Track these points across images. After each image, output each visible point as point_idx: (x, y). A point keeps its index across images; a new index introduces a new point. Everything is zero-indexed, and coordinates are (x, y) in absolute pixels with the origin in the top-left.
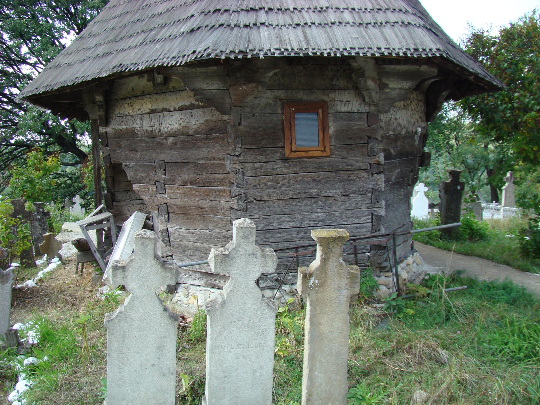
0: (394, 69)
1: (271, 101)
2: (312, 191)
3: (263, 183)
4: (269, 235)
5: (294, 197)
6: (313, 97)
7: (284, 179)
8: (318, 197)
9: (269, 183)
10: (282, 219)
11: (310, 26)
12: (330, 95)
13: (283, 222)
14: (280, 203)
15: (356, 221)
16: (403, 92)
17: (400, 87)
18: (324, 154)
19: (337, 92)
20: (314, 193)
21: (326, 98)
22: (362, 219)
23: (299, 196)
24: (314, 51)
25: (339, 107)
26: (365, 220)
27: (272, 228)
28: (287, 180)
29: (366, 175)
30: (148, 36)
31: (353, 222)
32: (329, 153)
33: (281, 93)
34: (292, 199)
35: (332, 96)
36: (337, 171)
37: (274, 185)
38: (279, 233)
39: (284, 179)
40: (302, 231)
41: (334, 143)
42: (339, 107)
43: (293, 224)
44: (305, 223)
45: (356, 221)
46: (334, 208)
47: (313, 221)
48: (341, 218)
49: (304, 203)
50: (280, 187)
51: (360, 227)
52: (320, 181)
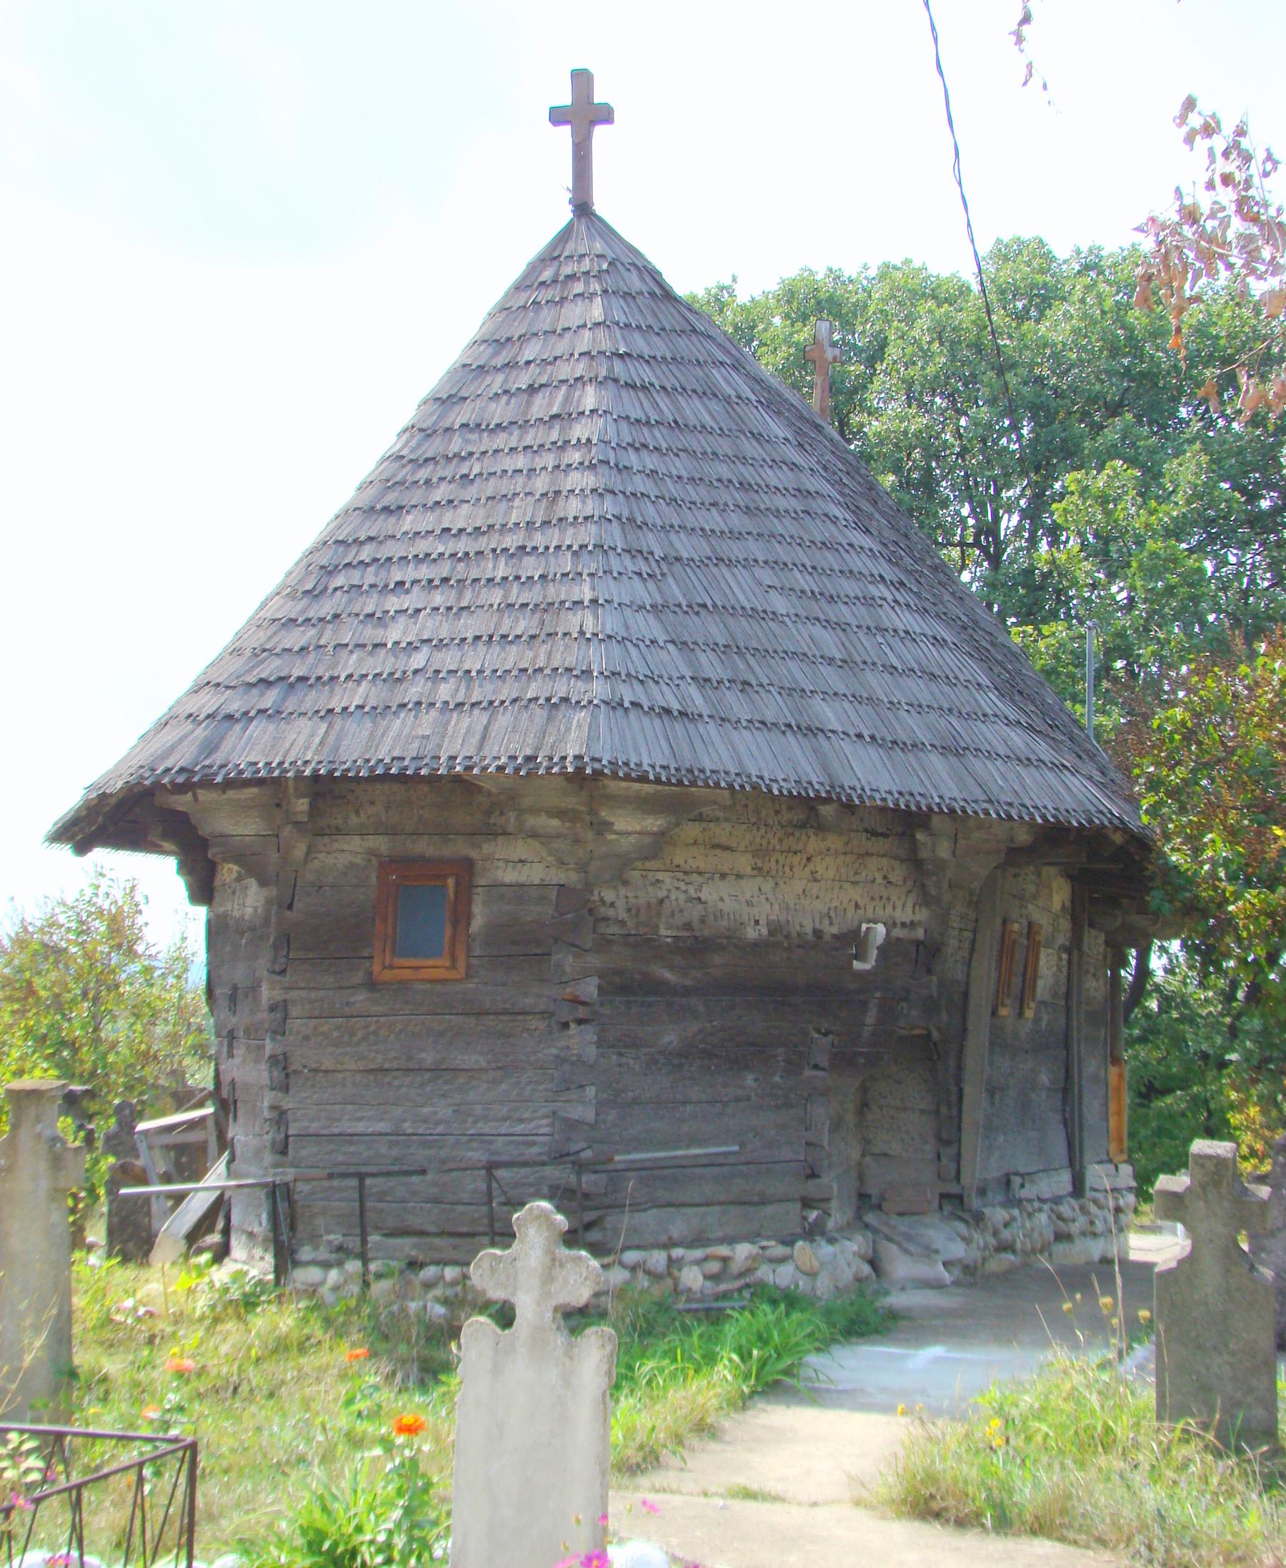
0: (627, 789)
1: (358, 860)
2: (423, 1055)
3: (322, 1034)
4: (331, 1147)
5: (387, 1066)
6: (447, 852)
7: (367, 1027)
8: (437, 1070)
9: (335, 1034)
10: (359, 1114)
11: (626, 710)
12: (485, 846)
13: (360, 1119)
14: (358, 1077)
15: (519, 1128)
16: (648, 840)
17: (638, 828)
18: (453, 975)
19: (500, 840)
20: (428, 1058)
21: (474, 854)
22: (531, 1126)
23: (395, 1065)
24: (597, 766)
25: (500, 873)
26: (539, 1127)
27: (336, 1131)
28: (373, 1028)
29: (542, 1025)
30: (186, 736)
31: (511, 1131)
32: (462, 970)
33: (381, 844)
34: (381, 1070)
35: (487, 848)
36: (480, 1014)
37: (346, 1038)
38: (351, 1143)
39: (367, 1027)
40: (398, 1143)
41: (477, 952)
42: (500, 873)
43: (381, 1126)
44: (406, 1125)
45: (519, 1128)
46: (472, 1096)
47: (425, 1121)
48: (486, 1119)
49: (407, 1080)
50: (358, 1044)
51: (524, 1143)
52: (442, 1034)
